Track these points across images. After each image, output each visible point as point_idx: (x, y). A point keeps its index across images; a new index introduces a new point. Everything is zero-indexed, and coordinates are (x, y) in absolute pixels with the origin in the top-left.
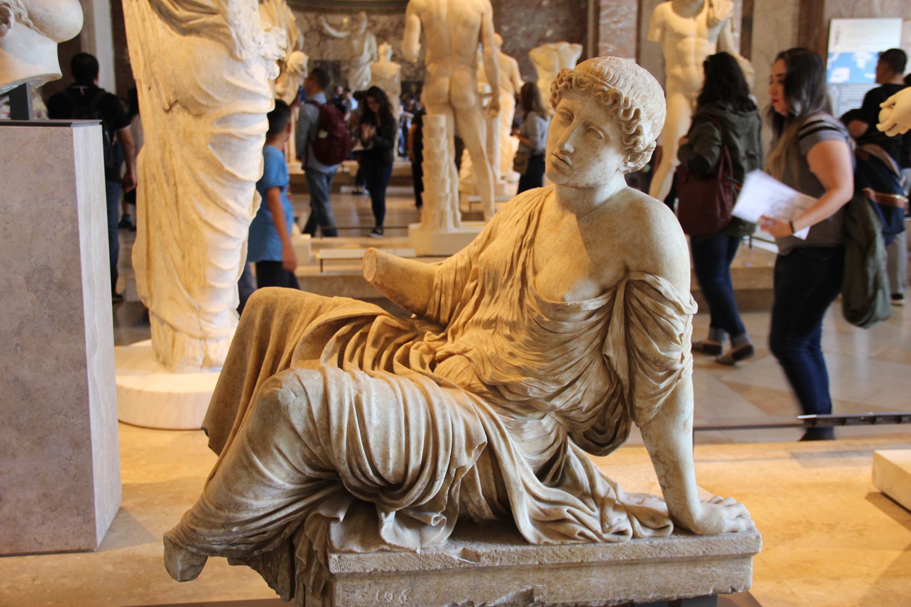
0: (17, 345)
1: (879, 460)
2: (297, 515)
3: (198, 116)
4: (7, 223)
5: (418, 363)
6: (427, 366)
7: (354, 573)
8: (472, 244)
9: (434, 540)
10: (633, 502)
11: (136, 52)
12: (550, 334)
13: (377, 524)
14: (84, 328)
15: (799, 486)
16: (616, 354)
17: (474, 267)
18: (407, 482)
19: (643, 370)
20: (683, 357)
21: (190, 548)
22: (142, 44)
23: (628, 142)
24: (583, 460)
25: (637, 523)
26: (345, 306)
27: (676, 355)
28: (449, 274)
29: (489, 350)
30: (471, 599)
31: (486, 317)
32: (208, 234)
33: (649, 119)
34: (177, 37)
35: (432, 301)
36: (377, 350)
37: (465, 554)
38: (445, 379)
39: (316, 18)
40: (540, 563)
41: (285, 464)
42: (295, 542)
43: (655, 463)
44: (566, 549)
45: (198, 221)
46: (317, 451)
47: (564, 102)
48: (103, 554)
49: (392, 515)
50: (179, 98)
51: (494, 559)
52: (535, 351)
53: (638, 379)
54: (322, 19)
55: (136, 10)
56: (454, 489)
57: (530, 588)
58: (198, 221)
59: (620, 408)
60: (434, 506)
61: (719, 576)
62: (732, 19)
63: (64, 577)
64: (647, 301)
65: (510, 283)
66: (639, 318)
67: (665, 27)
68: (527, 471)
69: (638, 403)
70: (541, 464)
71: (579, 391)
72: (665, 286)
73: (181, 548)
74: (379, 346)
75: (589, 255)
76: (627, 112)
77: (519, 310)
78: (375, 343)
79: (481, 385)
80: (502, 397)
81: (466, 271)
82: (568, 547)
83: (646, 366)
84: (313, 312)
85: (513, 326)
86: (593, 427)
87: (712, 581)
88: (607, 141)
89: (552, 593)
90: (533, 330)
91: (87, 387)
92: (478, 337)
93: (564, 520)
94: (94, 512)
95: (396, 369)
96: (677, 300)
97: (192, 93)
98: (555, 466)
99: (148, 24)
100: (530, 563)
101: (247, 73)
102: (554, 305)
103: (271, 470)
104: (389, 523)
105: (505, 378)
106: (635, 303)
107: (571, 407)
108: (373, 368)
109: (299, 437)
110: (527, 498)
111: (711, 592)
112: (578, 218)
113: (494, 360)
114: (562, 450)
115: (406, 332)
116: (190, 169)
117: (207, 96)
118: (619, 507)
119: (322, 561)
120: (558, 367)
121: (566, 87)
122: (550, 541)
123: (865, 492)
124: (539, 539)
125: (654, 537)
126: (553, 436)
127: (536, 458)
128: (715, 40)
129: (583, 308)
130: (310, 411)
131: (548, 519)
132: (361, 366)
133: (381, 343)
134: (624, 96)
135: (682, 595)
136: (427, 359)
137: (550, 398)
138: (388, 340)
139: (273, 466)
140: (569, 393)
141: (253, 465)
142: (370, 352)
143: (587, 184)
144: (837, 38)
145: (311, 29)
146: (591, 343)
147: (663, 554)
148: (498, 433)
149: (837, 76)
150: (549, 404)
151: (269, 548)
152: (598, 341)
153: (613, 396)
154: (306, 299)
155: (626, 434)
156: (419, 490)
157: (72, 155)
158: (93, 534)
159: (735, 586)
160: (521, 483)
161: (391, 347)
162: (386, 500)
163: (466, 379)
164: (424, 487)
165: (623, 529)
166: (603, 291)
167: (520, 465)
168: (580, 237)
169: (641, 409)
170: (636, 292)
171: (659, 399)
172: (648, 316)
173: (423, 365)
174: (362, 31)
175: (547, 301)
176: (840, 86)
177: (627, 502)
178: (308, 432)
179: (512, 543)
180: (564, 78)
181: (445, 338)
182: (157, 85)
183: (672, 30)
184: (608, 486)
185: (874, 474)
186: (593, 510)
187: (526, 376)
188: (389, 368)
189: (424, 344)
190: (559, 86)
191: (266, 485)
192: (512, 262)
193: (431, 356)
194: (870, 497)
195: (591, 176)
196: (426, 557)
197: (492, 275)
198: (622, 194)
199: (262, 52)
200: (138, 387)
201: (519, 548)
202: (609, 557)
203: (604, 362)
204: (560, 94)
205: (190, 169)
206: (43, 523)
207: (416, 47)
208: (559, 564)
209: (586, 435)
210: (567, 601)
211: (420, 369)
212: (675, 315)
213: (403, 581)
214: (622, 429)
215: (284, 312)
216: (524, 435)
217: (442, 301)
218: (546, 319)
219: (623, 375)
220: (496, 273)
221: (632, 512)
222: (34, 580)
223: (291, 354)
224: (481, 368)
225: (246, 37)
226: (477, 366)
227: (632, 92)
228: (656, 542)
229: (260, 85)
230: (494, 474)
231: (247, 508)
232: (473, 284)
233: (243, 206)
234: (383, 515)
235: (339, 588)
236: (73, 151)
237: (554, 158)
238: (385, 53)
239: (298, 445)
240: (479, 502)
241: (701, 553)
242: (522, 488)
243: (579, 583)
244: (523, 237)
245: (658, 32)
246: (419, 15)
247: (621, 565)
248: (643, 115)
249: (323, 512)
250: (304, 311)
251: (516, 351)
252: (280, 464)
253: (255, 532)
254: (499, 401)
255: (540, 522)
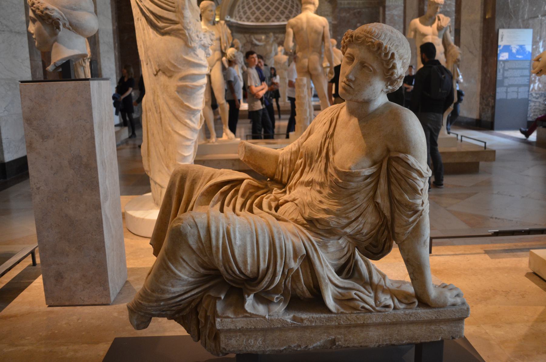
0: (66, 197)
1: (533, 255)
2: (198, 295)
3: (170, 77)
4: (59, 133)
5: (267, 207)
6: (273, 209)
7: (230, 329)
8: (300, 137)
9: (276, 310)
10: (394, 287)
11: (141, 46)
12: (343, 190)
13: (243, 301)
14: (99, 188)
15: (489, 269)
16: (382, 201)
17: (301, 150)
18: (260, 277)
19: (399, 210)
20: (423, 203)
21: (140, 313)
22: (143, 42)
23: (388, 74)
24: (366, 262)
25: (396, 301)
26: (226, 175)
27: (419, 202)
28: (287, 155)
29: (308, 199)
30: (300, 344)
31: (306, 180)
32: (176, 137)
33: (401, 59)
34: (159, 37)
35: (278, 170)
36: (244, 200)
37: (294, 319)
38: (282, 216)
39: (249, 37)
40: (339, 324)
41: (187, 267)
42: (198, 310)
43: (407, 265)
44: (354, 316)
45: (171, 131)
46: (206, 259)
47: (349, 50)
48: (114, 306)
49: (252, 296)
50: (161, 68)
51: (311, 322)
52: (334, 199)
53: (396, 215)
54: (252, 37)
55: (140, 24)
56: (287, 281)
57: (333, 337)
58: (171, 131)
59: (386, 233)
60: (276, 290)
61: (444, 330)
62: (450, 26)
63: (93, 319)
64: (400, 169)
65: (320, 160)
66: (396, 179)
67: (416, 31)
68: (330, 270)
69: (397, 230)
70: (339, 266)
71: (361, 223)
72: (411, 160)
73: (135, 312)
74: (246, 197)
75: (366, 142)
76: (386, 55)
77: (325, 175)
78: (243, 196)
79: (303, 220)
80: (315, 226)
81: (296, 153)
82: (355, 315)
83: (401, 208)
84: (208, 178)
85: (322, 185)
86: (370, 244)
87: (441, 333)
88: (375, 73)
89: (347, 341)
90: (332, 187)
91: (102, 219)
92: (302, 191)
93: (353, 299)
94: (108, 285)
95: (254, 211)
96: (419, 168)
97: (167, 65)
98: (348, 267)
99: (146, 32)
100: (333, 323)
101: (195, 54)
102: (345, 172)
103: (180, 271)
104: (250, 300)
105: (317, 216)
106: (394, 170)
107: (356, 232)
108: (241, 210)
109: (194, 252)
110: (330, 286)
111: (440, 339)
112: (359, 120)
113: (310, 205)
114: (352, 257)
115: (262, 189)
116: (167, 105)
117: (174, 66)
118: (386, 290)
119: (213, 322)
120: (348, 209)
121: (349, 41)
122: (345, 311)
123: (525, 273)
124: (338, 310)
125: (406, 308)
126: (346, 249)
127: (335, 262)
128: (442, 37)
129: (362, 174)
130: (199, 236)
131: (343, 298)
132: (234, 210)
133: (246, 196)
134: (385, 45)
135: (423, 341)
136: (273, 204)
137: (344, 227)
138: (251, 194)
139: (180, 268)
140: (354, 225)
141: (169, 268)
142: (240, 201)
143: (364, 99)
144: (502, 38)
145: (247, 42)
146: (368, 195)
147: (412, 319)
148: (313, 248)
149: (502, 57)
150: (343, 231)
151: (184, 313)
152: (371, 193)
153: (382, 225)
154: (205, 170)
155: (389, 249)
156: (266, 282)
157: (90, 96)
158: (108, 296)
159: (454, 336)
160: (327, 278)
161: (253, 197)
162: (248, 287)
163: (294, 216)
164: (269, 280)
165: (388, 304)
166: (374, 163)
167: (326, 267)
168: (360, 132)
169: (398, 234)
170: (394, 163)
171: (409, 228)
172: (402, 178)
173: (270, 208)
174: (271, 42)
175: (341, 170)
176: (504, 61)
177: (391, 287)
178: (199, 249)
179: (322, 313)
180: (348, 36)
181: (285, 192)
182: (151, 62)
183: (420, 32)
184: (380, 276)
185: (530, 262)
186: (370, 293)
187: (329, 214)
188: (251, 210)
189: (272, 196)
190: (346, 41)
191: (177, 279)
192: (321, 147)
193: (276, 202)
194: (528, 275)
195: (366, 94)
196: (272, 320)
197: (310, 155)
198: (385, 105)
199: (202, 43)
200: (142, 217)
201: (326, 315)
202: (379, 320)
203: (375, 206)
204: (347, 46)
205: (167, 105)
206: (84, 290)
207: (291, 44)
208: (350, 324)
209: (366, 248)
210: (355, 345)
211: (268, 210)
212: (418, 178)
213: (259, 333)
214: (387, 245)
215: (192, 179)
216: (329, 249)
217: (283, 171)
218: (340, 181)
219: (387, 213)
220: (312, 154)
221: (393, 294)
222: (78, 320)
223: (194, 202)
224: (303, 210)
225: (194, 35)
226: (301, 209)
227: (389, 43)
228: (407, 312)
229: (201, 60)
230: (311, 272)
231: (168, 292)
232: (300, 161)
233: (194, 123)
234: (246, 296)
235: (222, 337)
236: (90, 93)
237: (343, 84)
238: (281, 51)
239: (194, 256)
240: (302, 288)
241: (434, 318)
242: (327, 281)
243: (362, 335)
244: (327, 132)
245: (413, 33)
246: (292, 28)
247: (387, 324)
248: (396, 56)
249: (212, 293)
250: (203, 178)
251: (323, 200)
252: (184, 267)
253: (175, 305)
254: (313, 229)
255: (336, 300)
